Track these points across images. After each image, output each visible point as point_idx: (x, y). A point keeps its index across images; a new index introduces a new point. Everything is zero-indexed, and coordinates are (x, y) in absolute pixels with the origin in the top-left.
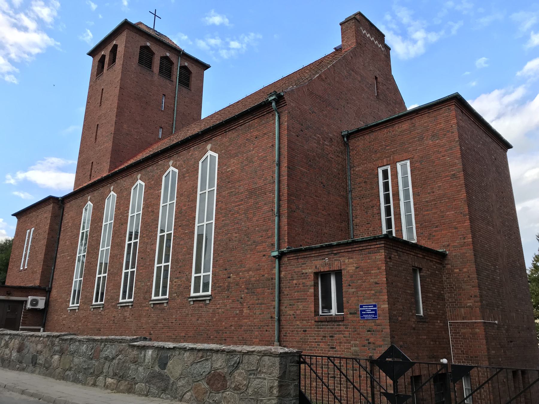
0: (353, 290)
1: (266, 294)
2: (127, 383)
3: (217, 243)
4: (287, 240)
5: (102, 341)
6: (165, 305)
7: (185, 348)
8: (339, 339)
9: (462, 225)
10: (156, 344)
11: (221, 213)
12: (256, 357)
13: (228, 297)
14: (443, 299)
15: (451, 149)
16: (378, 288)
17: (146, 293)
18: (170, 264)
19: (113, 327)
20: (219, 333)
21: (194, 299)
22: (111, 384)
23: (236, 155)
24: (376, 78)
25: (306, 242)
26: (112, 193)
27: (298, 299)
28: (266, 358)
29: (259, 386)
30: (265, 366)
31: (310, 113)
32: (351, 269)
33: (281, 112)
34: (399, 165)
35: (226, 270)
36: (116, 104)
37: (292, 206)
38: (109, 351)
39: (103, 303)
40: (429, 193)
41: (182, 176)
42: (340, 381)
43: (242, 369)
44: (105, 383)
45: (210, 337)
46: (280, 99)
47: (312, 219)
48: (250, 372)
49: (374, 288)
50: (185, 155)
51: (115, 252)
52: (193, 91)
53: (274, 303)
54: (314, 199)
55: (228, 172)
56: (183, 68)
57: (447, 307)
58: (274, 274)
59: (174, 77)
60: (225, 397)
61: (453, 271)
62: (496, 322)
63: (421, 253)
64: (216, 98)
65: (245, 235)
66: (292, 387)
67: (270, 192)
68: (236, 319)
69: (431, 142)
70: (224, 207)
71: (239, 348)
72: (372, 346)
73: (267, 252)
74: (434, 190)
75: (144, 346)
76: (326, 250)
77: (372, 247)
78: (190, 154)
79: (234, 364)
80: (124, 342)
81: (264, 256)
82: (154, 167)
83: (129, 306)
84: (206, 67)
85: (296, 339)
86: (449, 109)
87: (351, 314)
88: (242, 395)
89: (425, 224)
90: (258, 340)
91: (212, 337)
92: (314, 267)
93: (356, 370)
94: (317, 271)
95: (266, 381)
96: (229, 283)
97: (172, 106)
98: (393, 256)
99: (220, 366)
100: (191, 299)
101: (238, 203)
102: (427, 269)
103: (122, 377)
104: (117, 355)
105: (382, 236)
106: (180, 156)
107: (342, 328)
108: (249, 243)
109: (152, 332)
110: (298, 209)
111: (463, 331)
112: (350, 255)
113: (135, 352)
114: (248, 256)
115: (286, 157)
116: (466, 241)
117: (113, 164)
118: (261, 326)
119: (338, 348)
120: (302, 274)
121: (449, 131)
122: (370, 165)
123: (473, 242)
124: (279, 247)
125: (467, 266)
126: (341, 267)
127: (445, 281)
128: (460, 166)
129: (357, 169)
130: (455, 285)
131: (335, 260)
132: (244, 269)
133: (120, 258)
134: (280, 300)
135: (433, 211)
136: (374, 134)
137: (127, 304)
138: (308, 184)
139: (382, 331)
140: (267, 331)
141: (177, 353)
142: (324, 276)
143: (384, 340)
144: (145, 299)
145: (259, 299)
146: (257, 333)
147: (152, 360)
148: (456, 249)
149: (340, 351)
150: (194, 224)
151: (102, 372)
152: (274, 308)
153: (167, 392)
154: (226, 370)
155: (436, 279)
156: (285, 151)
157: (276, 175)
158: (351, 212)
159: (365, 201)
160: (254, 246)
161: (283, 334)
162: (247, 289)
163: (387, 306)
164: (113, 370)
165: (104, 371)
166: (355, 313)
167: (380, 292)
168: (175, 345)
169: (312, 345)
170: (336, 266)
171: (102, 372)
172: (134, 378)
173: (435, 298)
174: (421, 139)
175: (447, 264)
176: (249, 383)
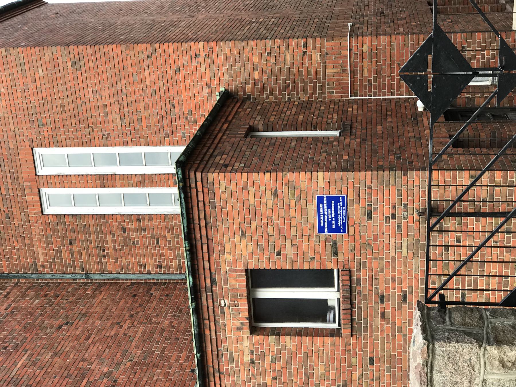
8: (387, 284)
14: (310, 103)
16: (286, 191)
25: (185, 361)
27: (306, 375)
40: (106, 115)
47: (137, 347)
49: (286, 199)
57: (325, 98)
61: (257, 82)
62: (349, 24)
72: (399, 212)
74: (100, 104)
76: (205, 303)
77: (201, 198)
87: (336, 254)
94: (247, 326)
98: (222, 162)
102: (253, 120)
105: (180, 172)
107: (364, 274)
110: (108, 374)
111: (366, 73)
112: (216, 249)
116: (202, 54)
119: (404, 286)
120: (253, 362)
122: (37, 231)
123: (208, 40)
125: (250, 55)
126: (241, 271)
128: (57, 51)
129: (42, 259)
130: (284, 81)
131: (226, 283)
135: (142, 109)
138: (56, 354)
139: (370, 188)
143: (388, 185)
148: (216, 72)
155: (271, 109)
158: (131, 277)
159: (110, 245)
163: (320, 175)
166: (335, 243)
167: (293, 186)
169: (399, 345)
170: (238, 283)
173: (308, 114)
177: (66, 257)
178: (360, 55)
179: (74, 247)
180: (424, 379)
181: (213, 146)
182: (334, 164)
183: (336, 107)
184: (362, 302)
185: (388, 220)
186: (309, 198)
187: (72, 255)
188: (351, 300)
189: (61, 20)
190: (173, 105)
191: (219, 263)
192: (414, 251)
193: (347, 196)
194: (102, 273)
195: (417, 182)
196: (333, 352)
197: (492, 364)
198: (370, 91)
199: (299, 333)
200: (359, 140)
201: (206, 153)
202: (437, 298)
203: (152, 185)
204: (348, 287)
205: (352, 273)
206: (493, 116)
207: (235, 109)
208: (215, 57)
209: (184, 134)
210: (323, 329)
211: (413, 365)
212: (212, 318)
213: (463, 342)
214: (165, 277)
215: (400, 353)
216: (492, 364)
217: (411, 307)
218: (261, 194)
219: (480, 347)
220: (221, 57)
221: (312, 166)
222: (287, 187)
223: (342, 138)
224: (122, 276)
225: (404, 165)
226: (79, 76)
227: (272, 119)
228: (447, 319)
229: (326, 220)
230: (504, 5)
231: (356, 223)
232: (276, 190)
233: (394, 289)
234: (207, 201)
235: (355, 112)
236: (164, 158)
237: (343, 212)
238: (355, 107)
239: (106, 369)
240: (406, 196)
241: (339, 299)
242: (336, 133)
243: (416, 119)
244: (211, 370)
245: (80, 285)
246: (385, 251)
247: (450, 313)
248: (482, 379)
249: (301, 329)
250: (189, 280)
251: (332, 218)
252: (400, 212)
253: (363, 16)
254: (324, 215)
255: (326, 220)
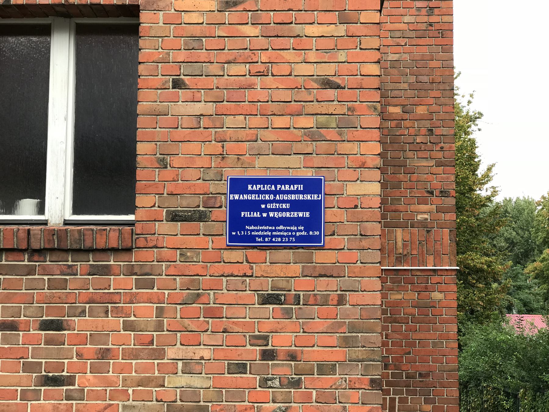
0: (198, 108)
72: (281, 369)
87: (174, 217)
107: (120, 283)
116: (433, 19)
139: (341, 301)
143: (347, 342)
148: (402, 42)
163: (375, 188)
166: (202, 217)
167: (345, 124)
178: (426, 287)
184: (46, 278)
185: (260, 342)
186: (317, 161)
188: (52, 250)
192: (179, 403)
193: (322, 248)
204: (88, 244)
205: (125, 256)
208: (427, 41)
217: (30, 395)
220: (425, 50)
222: (345, 111)
229: (262, 197)
231: (252, 268)
232: (338, 87)
233: (79, 355)
237: (282, 237)
240: (319, 384)
246: (179, 334)
251: (267, 210)
252: (280, 371)
254: (275, 193)
255: (262, 197)
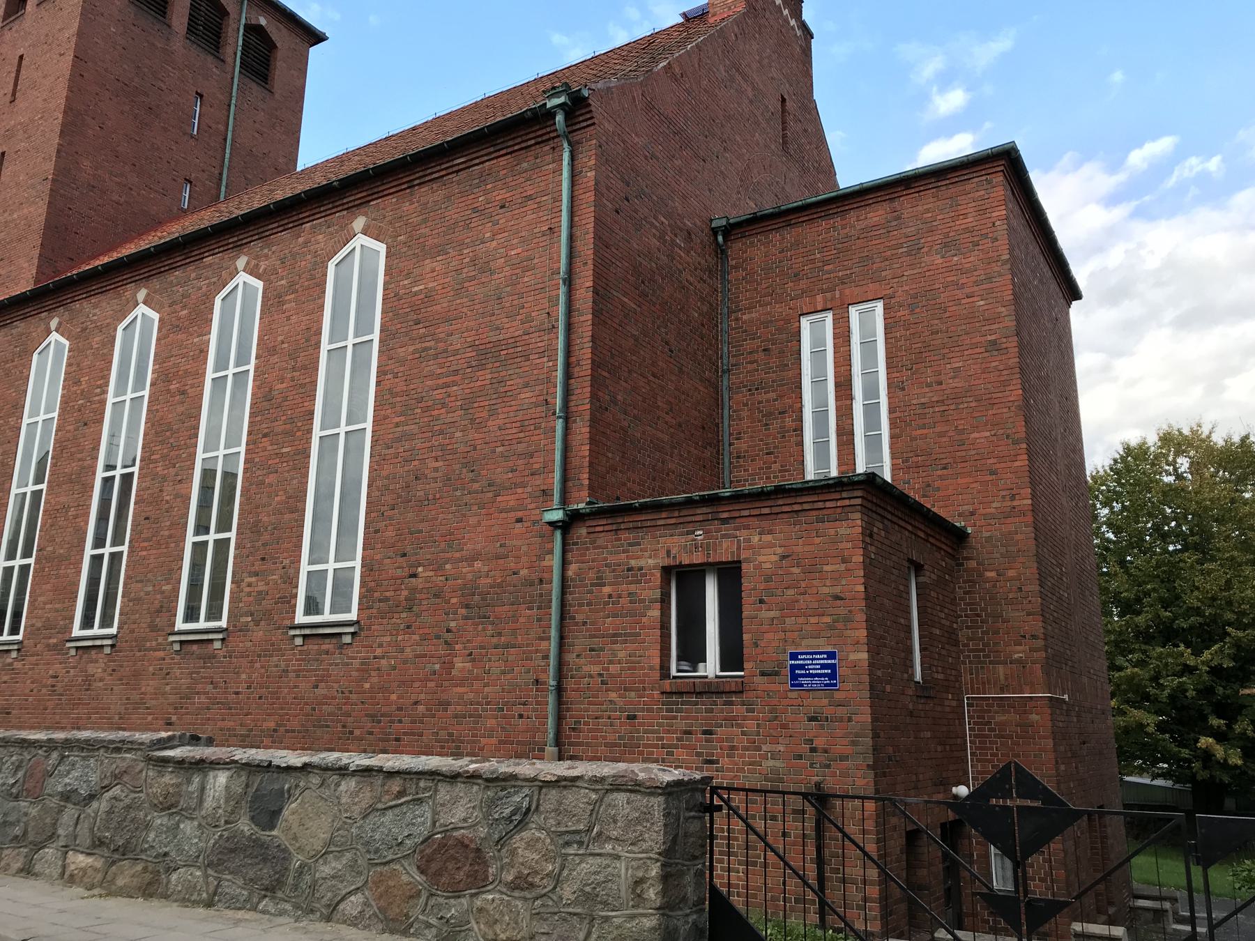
0: (772, 614)
1: (522, 620)
2: (139, 867)
3: (379, 483)
4: (586, 482)
5: (51, 745)
6: (217, 645)
7: (346, 768)
8: (727, 740)
9: (1009, 464)
10: (241, 755)
11: (393, 405)
12: (586, 796)
13: (408, 627)
15: (989, 279)
16: (843, 611)
17: (159, 611)
18: (232, 535)
19: (50, 704)
20: (379, 722)
21: (307, 632)
22: (84, 870)
23: (440, 251)
24: (784, 100)
26: (55, 336)
27: (615, 635)
28: (621, 798)
29: (600, 878)
30: (615, 822)
31: (646, 157)
32: (768, 559)
33: (578, 143)
34: (854, 312)
35: (404, 555)
36: (63, 101)
37: (600, 394)
38: (78, 775)
39: (20, 637)
40: (929, 385)
41: (272, 302)
42: (729, 846)
43: (540, 828)
44: (64, 867)
45: (351, 733)
46: (577, 106)
47: (644, 433)
48: (567, 838)
50: (285, 243)
51: (63, 499)
52: (276, 96)
53: (544, 644)
54: (649, 382)
55: (416, 294)
56: (254, 30)
58: (550, 569)
59: (229, 50)
60: (480, 910)
61: (981, 575)
62: (1066, 697)
63: (923, 527)
64: (338, 119)
65: (465, 465)
66: (689, 878)
67: (541, 354)
68: (432, 684)
69: (940, 261)
70: (401, 386)
71: (526, 768)
72: (819, 757)
73: (527, 513)
74: (943, 377)
75: (202, 761)
76: (699, 511)
77: (828, 504)
78: (301, 240)
79: (513, 813)
80: (129, 750)
81: (519, 520)
82: (191, 272)
83: (102, 646)
84: (316, 38)
85: (605, 738)
86: (989, 182)
87: (763, 674)
88: (538, 902)
89: (915, 459)
90: (494, 740)
91: (357, 732)
92: (663, 553)
93: (774, 818)
95: (622, 866)
96: (414, 590)
97: (221, 127)
98: (875, 530)
99: (465, 820)
100: (297, 632)
101: (445, 380)
103: (124, 851)
104: (106, 788)
106: (269, 246)
107: (739, 710)
108: (476, 486)
109: (174, 718)
110: (614, 401)
111: (999, 718)
112: (765, 524)
113: (169, 779)
114: (473, 521)
115: (590, 262)
116: (1015, 503)
117: (46, 259)
118: (506, 704)
119: (725, 762)
120: (629, 570)
121: (985, 236)
122: (780, 309)
123: (1034, 509)
124: (564, 501)
126: (739, 555)
127: (962, 599)
128: (1010, 323)
130: (984, 609)
131: (723, 536)
132: (458, 555)
133: (76, 517)
134: (562, 638)
135: (938, 429)
136: (794, 231)
137: (98, 643)
139: (850, 720)
140: (521, 716)
141: (315, 780)
142: (686, 579)
143: (854, 743)
144: (153, 628)
145: (500, 634)
146: (491, 723)
147: (227, 801)
148: (993, 522)
149: (729, 770)
150: (310, 431)
151: (53, 836)
152: (546, 657)
153: (279, 894)
154: (483, 831)
156: (586, 248)
157: (562, 308)
158: (726, 423)
159: (764, 397)
160: (490, 495)
161: (569, 722)
162: (467, 606)
163: (865, 656)
164: (91, 830)
165: (61, 831)
166: (777, 674)
167: (848, 620)
168: (306, 759)
170: (725, 552)
171: (53, 836)
172: (166, 854)
173: (940, 641)
174: (915, 251)
175: (968, 559)
176: (563, 868)
177: (748, 345)
179: (761, 354)
180: (619, 781)
181: (895, 519)
182: (879, 673)
183: (952, 678)
187: (751, 353)
189: (1049, 325)
190: (945, 468)
191: (747, 527)
194: (730, 389)
195: (860, 782)
196: (643, 668)
197: (638, 868)
198: (975, 723)
199: (665, 626)
200: (911, 706)
201: (885, 509)
202: (716, 802)
203: (839, 444)
206: (949, 889)
207: (944, 547)
209: (909, 483)
210: (669, 656)
211: (636, 767)
212: (681, 520)
213: (665, 833)
214: (727, 464)
215: (641, 753)
216: (638, 868)
218: (836, 579)
219: (660, 854)
221: (875, 646)
223: (912, 685)
224: (726, 412)
225: (880, 767)
226: (978, 350)
227: (933, 594)
228: (692, 814)
230: (1106, 913)
234: (825, 512)
235: (947, 703)
236: (876, 456)
238: (954, 703)
239: (619, 397)
241: (706, 677)
242: (918, 677)
243: (941, 784)
244: (620, 520)
245: (715, 364)
247: (700, 818)
248: (621, 854)
249: (669, 629)
250: (726, 492)
253: (1078, 716)
